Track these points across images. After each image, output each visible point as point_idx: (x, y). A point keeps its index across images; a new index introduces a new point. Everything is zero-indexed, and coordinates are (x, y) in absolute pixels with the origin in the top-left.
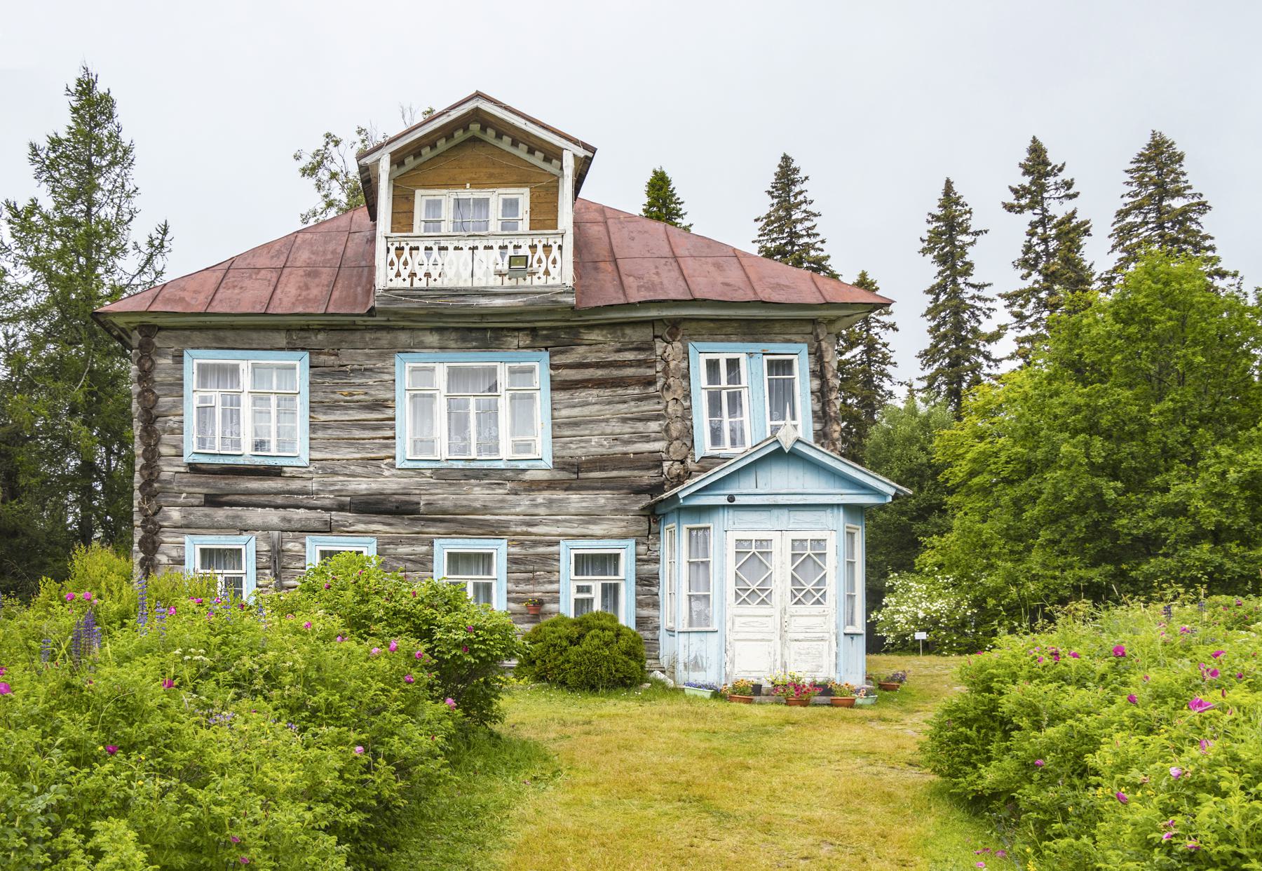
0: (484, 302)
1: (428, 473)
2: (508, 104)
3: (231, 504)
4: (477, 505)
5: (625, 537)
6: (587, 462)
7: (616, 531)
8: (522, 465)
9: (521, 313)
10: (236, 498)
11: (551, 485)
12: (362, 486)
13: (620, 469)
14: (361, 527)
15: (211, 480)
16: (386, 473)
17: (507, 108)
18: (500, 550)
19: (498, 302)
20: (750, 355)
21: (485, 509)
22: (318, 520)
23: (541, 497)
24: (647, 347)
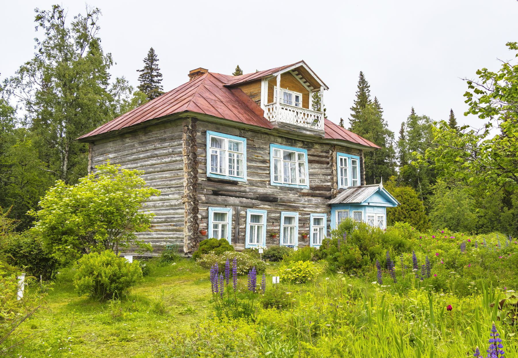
0: (304, 132)
1: (279, 187)
2: (310, 67)
3: (222, 195)
4: (292, 200)
5: (323, 213)
6: (315, 187)
7: (323, 211)
8: (302, 187)
9: (314, 137)
10: (224, 192)
11: (308, 195)
12: (261, 190)
13: (322, 190)
14: (262, 206)
15: (215, 184)
16: (268, 187)
17: (309, 68)
18: (296, 215)
19: (308, 133)
20: (349, 158)
21: (294, 202)
22: (251, 203)
23: (306, 198)
24: (327, 152)
